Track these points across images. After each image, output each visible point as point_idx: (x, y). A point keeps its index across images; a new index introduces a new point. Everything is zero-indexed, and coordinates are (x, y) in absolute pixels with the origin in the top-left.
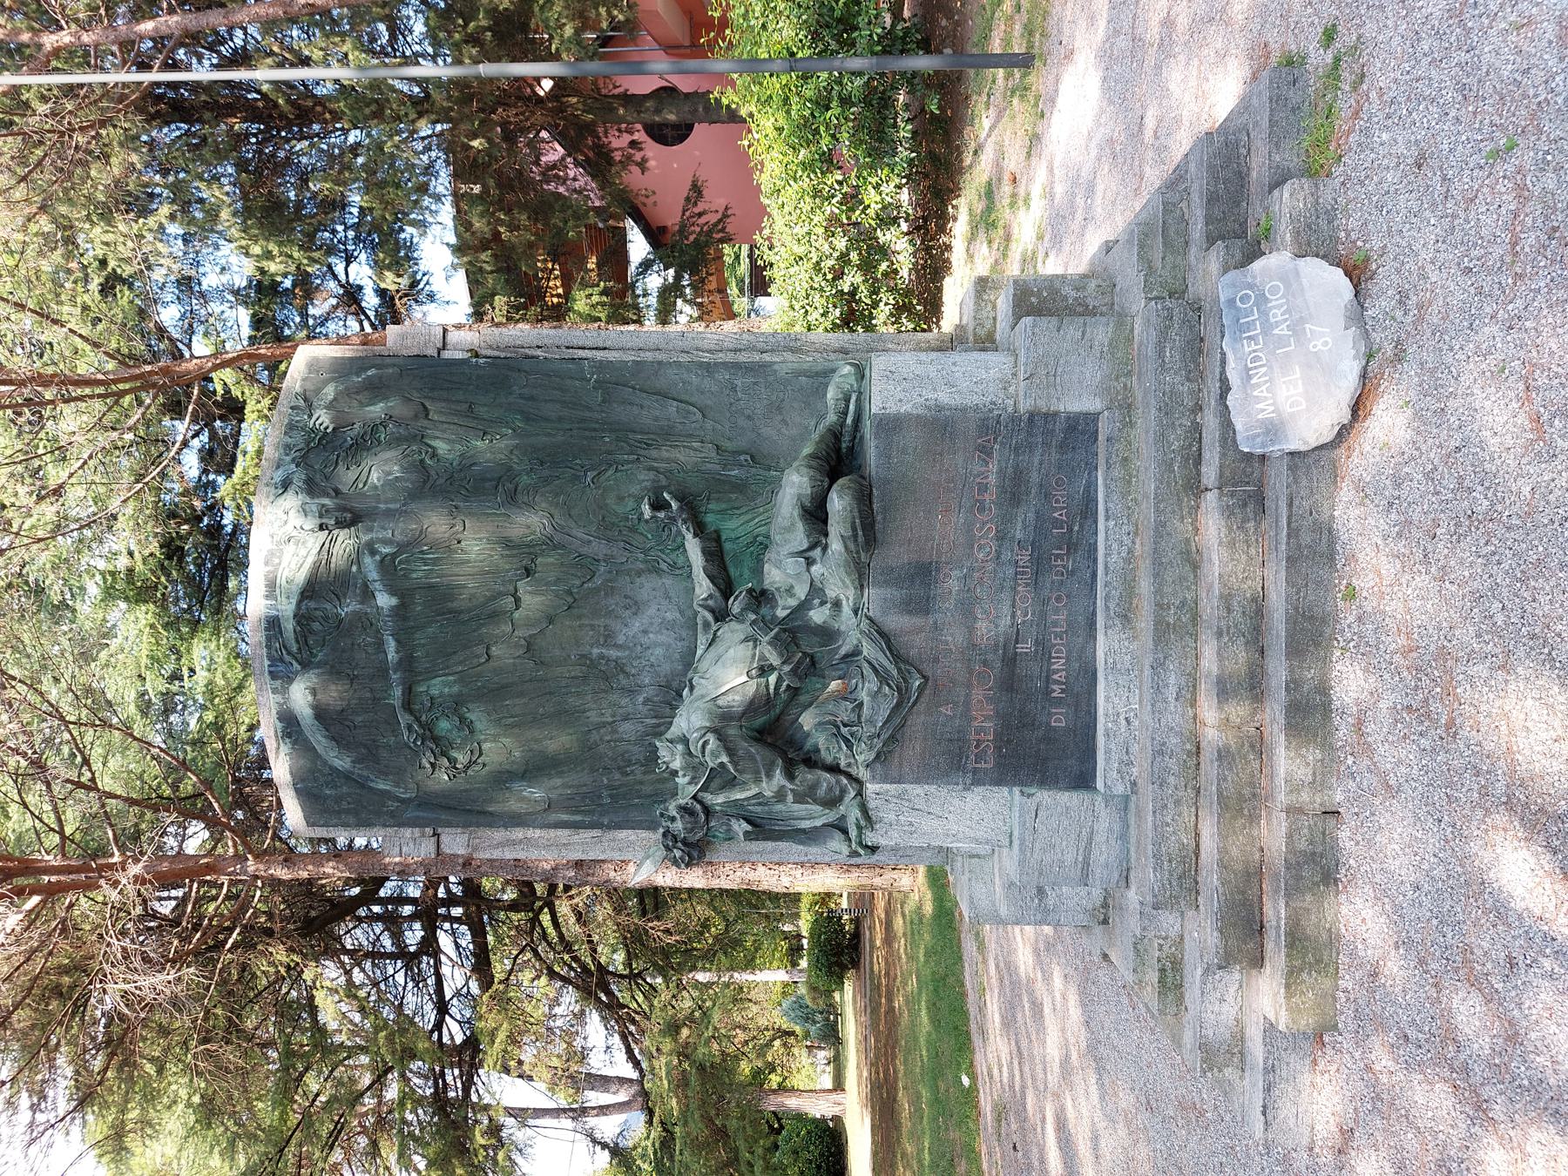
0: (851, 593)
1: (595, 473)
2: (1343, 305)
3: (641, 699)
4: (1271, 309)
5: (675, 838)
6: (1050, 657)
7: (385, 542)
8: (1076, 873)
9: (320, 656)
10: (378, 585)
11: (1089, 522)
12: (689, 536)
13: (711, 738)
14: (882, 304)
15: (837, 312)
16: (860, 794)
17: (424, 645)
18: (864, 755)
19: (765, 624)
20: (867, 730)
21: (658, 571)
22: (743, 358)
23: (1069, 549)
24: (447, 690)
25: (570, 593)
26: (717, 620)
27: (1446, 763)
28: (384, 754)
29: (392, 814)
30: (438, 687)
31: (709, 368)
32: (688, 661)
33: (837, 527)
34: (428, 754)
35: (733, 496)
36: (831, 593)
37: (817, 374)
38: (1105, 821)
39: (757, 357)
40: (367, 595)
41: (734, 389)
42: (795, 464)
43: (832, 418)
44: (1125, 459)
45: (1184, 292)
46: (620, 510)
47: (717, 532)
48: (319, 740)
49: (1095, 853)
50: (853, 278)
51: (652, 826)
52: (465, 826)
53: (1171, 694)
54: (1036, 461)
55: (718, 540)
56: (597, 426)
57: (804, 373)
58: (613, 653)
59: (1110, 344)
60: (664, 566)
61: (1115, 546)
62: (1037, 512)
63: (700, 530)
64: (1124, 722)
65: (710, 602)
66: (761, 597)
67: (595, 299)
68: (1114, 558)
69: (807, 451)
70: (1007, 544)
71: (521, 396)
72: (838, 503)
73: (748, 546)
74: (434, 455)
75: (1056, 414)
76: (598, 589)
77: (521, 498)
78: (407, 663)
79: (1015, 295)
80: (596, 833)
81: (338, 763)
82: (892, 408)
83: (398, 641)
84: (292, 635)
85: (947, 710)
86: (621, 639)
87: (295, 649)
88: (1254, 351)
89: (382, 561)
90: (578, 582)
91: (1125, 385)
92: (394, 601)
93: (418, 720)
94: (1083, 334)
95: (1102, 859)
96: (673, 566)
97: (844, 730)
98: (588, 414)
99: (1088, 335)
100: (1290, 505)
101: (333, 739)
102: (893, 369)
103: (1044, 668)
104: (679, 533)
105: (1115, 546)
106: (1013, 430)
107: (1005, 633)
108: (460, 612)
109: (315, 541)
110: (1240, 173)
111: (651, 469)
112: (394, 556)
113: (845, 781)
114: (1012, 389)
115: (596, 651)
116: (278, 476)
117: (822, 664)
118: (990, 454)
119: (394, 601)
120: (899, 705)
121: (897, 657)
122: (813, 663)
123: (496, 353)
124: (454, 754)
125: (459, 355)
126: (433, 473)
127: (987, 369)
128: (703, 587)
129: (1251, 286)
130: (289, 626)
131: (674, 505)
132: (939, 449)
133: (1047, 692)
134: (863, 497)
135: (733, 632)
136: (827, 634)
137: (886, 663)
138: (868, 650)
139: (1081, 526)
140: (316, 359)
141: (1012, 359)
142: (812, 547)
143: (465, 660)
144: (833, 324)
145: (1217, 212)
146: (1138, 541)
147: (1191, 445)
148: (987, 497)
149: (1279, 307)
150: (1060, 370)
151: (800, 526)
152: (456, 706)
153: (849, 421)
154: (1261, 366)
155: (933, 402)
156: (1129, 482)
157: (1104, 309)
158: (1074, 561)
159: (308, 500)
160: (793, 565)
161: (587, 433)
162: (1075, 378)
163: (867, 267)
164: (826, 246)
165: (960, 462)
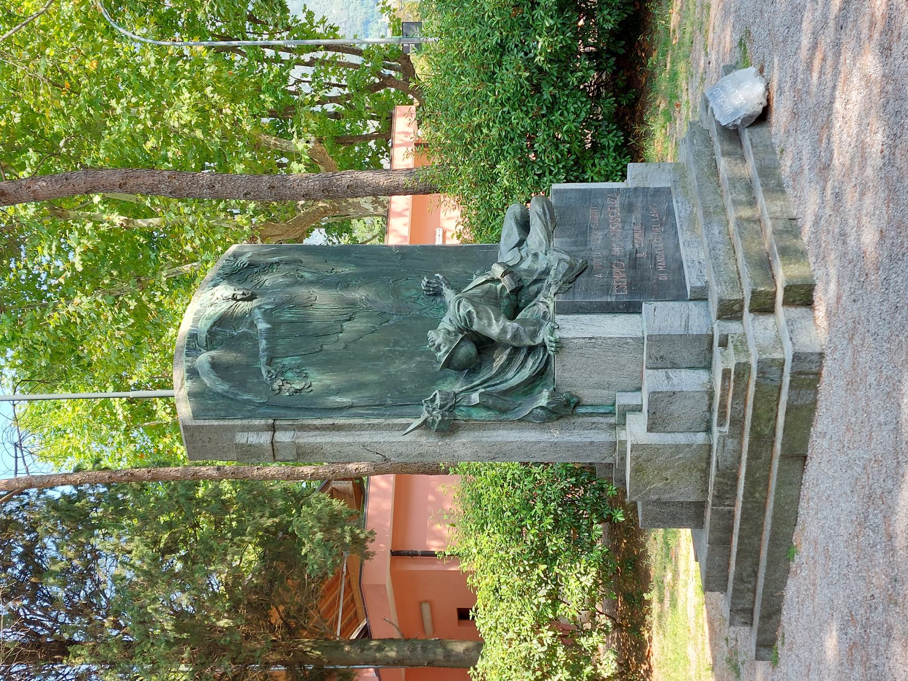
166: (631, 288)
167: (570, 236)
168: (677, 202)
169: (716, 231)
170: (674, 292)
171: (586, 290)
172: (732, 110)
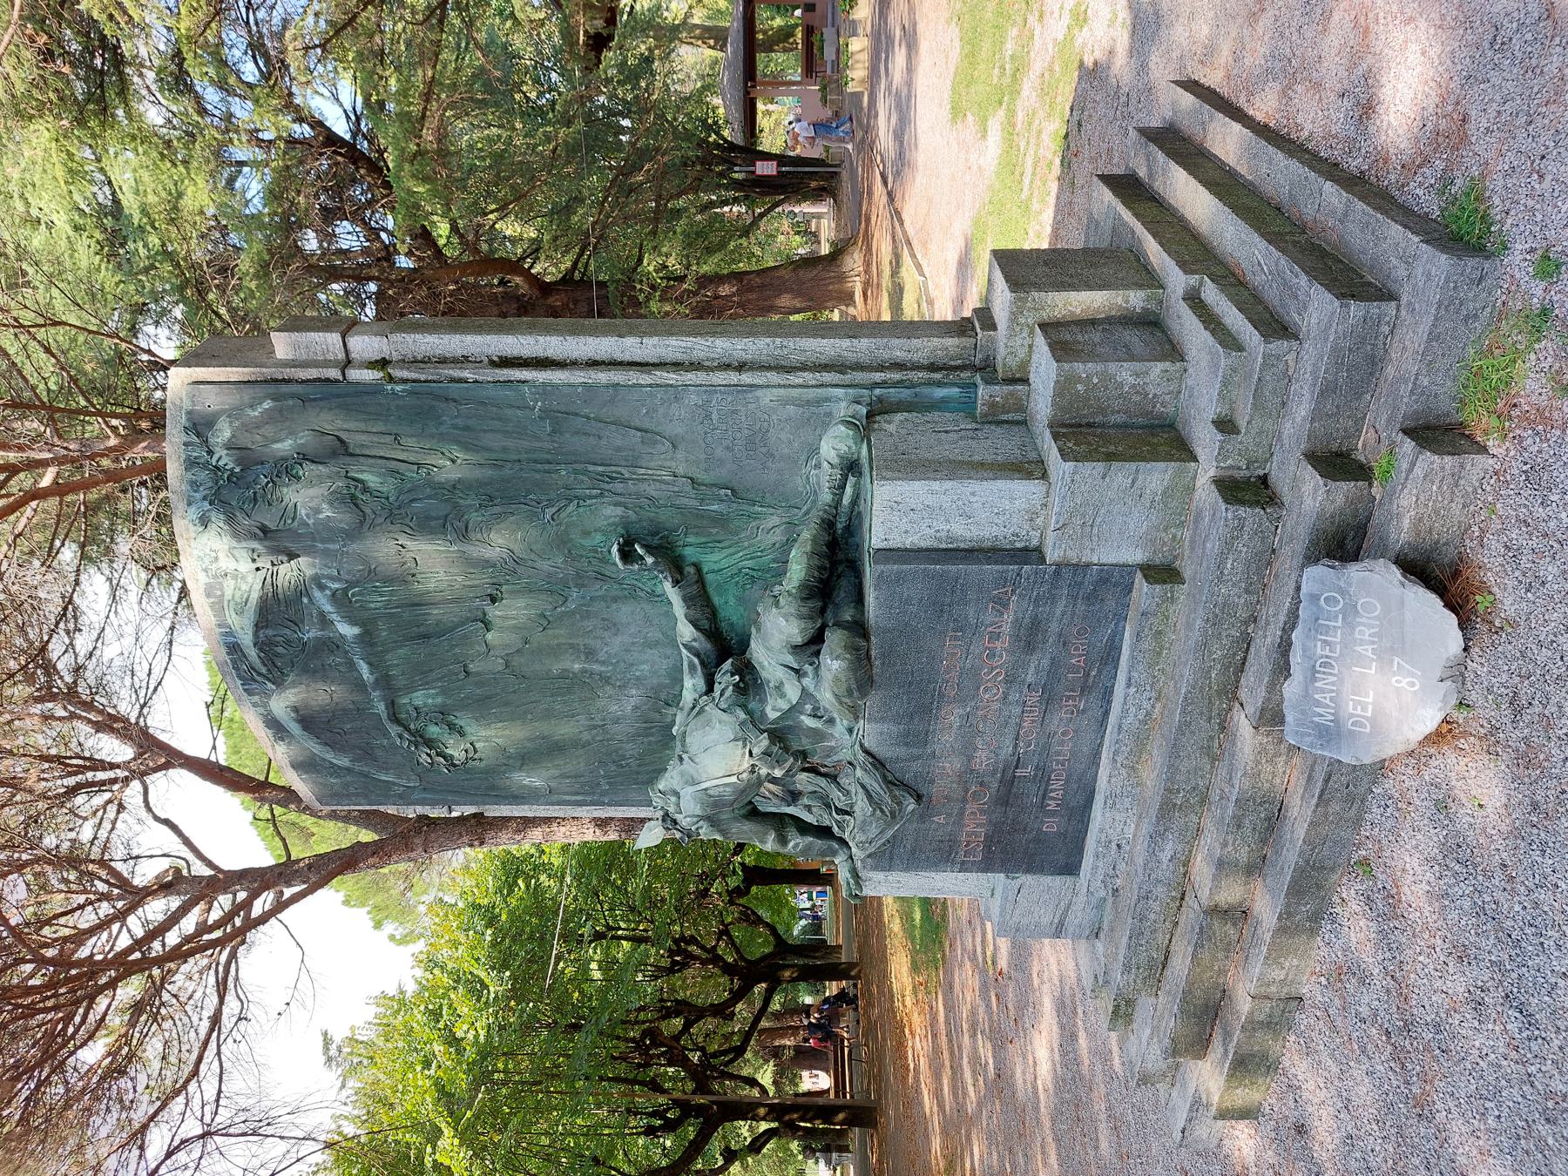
1: (554, 510)
2: (1445, 656)
4: (1360, 624)
6: (1049, 779)
10: (334, 616)
11: (1108, 668)
17: (398, 665)
19: (755, 721)
23: (1082, 691)
24: (430, 701)
27: (1456, 282)
28: (379, 753)
29: (400, 796)
35: (714, 531)
45: (1266, 461)
46: (587, 542)
49: (1071, 917)
54: (1058, 612)
55: (701, 580)
56: (549, 457)
59: (1164, 493)
61: (1133, 709)
62: (1053, 659)
64: (1115, 847)
68: (1130, 720)
70: (1016, 686)
71: (455, 427)
75: (1088, 565)
76: (573, 613)
77: (472, 535)
78: (384, 681)
79: (1057, 382)
83: (369, 664)
84: (258, 661)
85: (941, 819)
86: (602, 656)
88: (1327, 657)
89: (334, 595)
91: (1174, 537)
92: (356, 630)
93: (407, 729)
94: (1133, 482)
95: (1076, 921)
98: (537, 444)
99: (1139, 483)
100: (1327, 781)
101: (326, 744)
102: (899, 499)
103: (1042, 788)
105: (1133, 709)
106: (1035, 583)
107: (1006, 761)
110: (1373, 356)
112: (345, 590)
114: (1039, 521)
118: (1006, 606)
119: (356, 630)
126: (368, 511)
127: (1012, 499)
129: (1342, 592)
132: (948, 600)
133: (1042, 806)
139: (1100, 672)
141: (1044, 489)
143: (443, 677)
145: (1329, 407)
146: (1158, 705)
147: (1235, 654)
148: (998, 644)
149: (1370, 626)
150: (1099, 520)
152: (443, 715)
154: (1331, 674)
155: (943, 534)
156: (1159, 654)
157: (1167, 398)
158: (1087, 702)
159: (235, 544)
162: (1116, 529)
165: (972, 612)
166: (990, 847)
167: (897, 720)
168: (1129, 685)
169: (1165, 856)
170: (1061, 859)
171: (913, 851)
172: (1326, 719)
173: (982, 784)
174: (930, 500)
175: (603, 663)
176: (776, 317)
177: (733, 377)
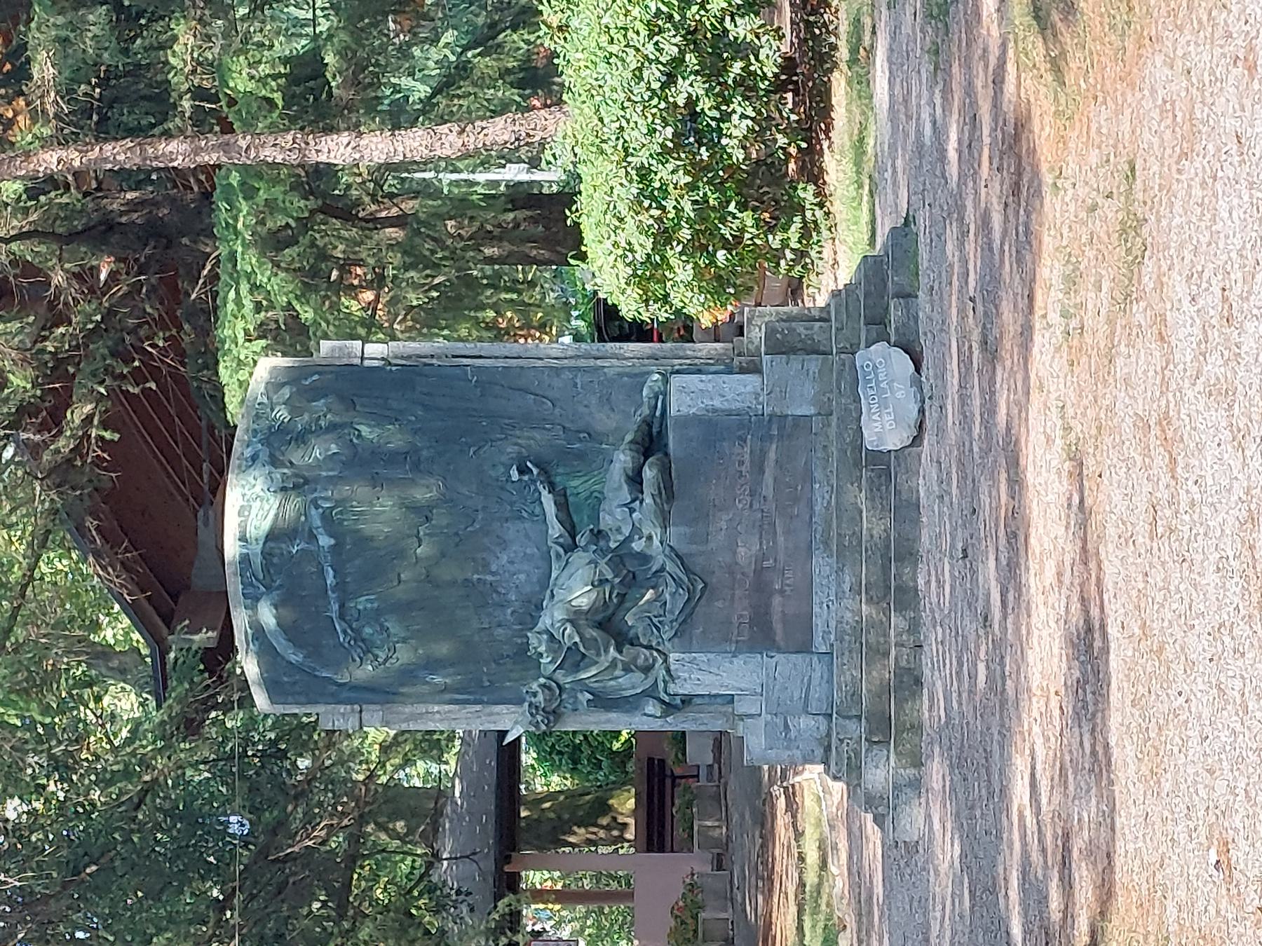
0: (659, 531)
3: (509, 611)
5: (537, 707)
7: (326, 499)
8: (801, 705)
9: (278, 582)
12: (545, 493)
13: (568, 625)
14: (735, 117)
15: (669, 131)
16: (665, 661)
18: (667, 633)
19: (603, 552)
20: (669, 617)
21: (521, 518)
22: (582, 363)
25: (457, 534)
26: (566, 552)
30: (362, 603)
31: (557, 371)
32: (545, 582)
33: (648, 489)
34: (359, 650)
36: (646, 532)
37: (636, 375)
38: (819, 669)
39: (592, 362)
40: (313, 537)
41: (575, 385)
42: (622, 447)
43: (646, 411)
44: (825, 447)
47: (565, 489)
48: (281, 644)
50: (688, 87)
51: (519, 702)
52: (382, 704)
53: (846, 587)
57: (629, 375)
58: (489, 578)
60: (525, 515)
63: (552, 488)
65: (561, 540)
66: (598, 535)
67: (264, 69)
69: (629, 437)
71: (421, 393)
72: (649, 473)
73: (586, 499)
74: (359, 436)
75: (787, 416)
78: (340, 586)
80: (478, 707)
81: (293, 658)
82: (684, 410)
83: (334, 570)
85: (719, 604)
86: (494, 568)
87: (261, 577)
90: (463, 527)
92: (332, 542)
96: (533, 514)
97: (655, 620)
101: (289, 640)
104: (536, 490)
108: (378, 549)
109: (274, 502)
111: (516, 444)
112: (332, 508)
113: (655, 654)
115: (476, 576)
116: (248, 453)
117: (640, 577)
119: (332, 542)
120: (689, 599)
121: (687, 571)
122: (634, 577)
123: (404, 362)
124: (377, 652)
125: (376, 363)
128: (555, 529)
130: (257, 561)
131: (535, 471)
134: (665, 470)
135: (579, 558)
136: (644, 558)
137: (681, 575)
138: (669, 567)
140: (275, 368)
142: (633, 501)
144: (663, 146)
148: (743, 469)
151: (625, 487)
153: (658, 413)
160: (620, 513)
161: (965, 695)
163: (713, 71)
164: (650, 47)
173: (743, 574)
174: (701, 386)
175: (493, 574)
176: (567, 850)
177: (592, 362)
